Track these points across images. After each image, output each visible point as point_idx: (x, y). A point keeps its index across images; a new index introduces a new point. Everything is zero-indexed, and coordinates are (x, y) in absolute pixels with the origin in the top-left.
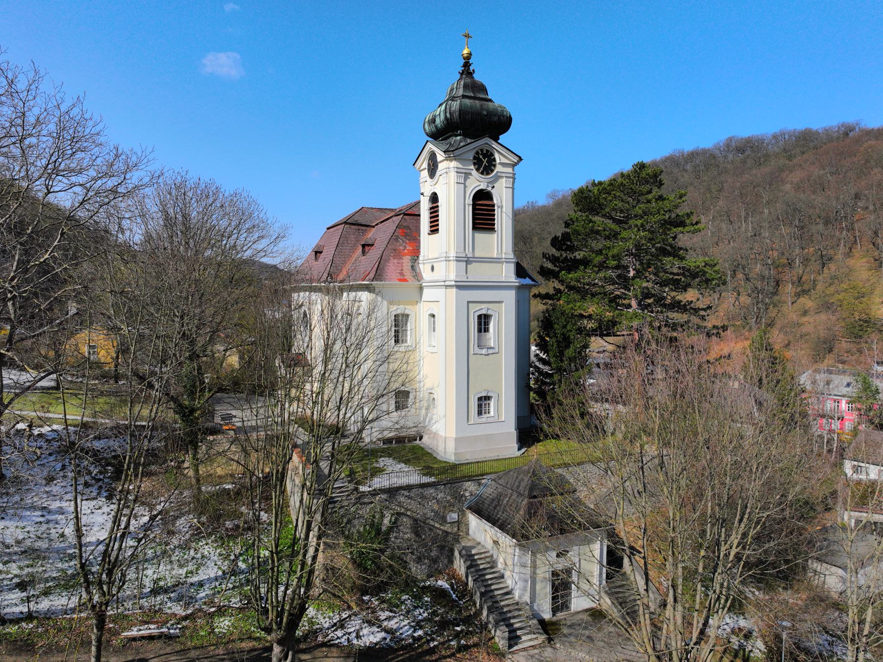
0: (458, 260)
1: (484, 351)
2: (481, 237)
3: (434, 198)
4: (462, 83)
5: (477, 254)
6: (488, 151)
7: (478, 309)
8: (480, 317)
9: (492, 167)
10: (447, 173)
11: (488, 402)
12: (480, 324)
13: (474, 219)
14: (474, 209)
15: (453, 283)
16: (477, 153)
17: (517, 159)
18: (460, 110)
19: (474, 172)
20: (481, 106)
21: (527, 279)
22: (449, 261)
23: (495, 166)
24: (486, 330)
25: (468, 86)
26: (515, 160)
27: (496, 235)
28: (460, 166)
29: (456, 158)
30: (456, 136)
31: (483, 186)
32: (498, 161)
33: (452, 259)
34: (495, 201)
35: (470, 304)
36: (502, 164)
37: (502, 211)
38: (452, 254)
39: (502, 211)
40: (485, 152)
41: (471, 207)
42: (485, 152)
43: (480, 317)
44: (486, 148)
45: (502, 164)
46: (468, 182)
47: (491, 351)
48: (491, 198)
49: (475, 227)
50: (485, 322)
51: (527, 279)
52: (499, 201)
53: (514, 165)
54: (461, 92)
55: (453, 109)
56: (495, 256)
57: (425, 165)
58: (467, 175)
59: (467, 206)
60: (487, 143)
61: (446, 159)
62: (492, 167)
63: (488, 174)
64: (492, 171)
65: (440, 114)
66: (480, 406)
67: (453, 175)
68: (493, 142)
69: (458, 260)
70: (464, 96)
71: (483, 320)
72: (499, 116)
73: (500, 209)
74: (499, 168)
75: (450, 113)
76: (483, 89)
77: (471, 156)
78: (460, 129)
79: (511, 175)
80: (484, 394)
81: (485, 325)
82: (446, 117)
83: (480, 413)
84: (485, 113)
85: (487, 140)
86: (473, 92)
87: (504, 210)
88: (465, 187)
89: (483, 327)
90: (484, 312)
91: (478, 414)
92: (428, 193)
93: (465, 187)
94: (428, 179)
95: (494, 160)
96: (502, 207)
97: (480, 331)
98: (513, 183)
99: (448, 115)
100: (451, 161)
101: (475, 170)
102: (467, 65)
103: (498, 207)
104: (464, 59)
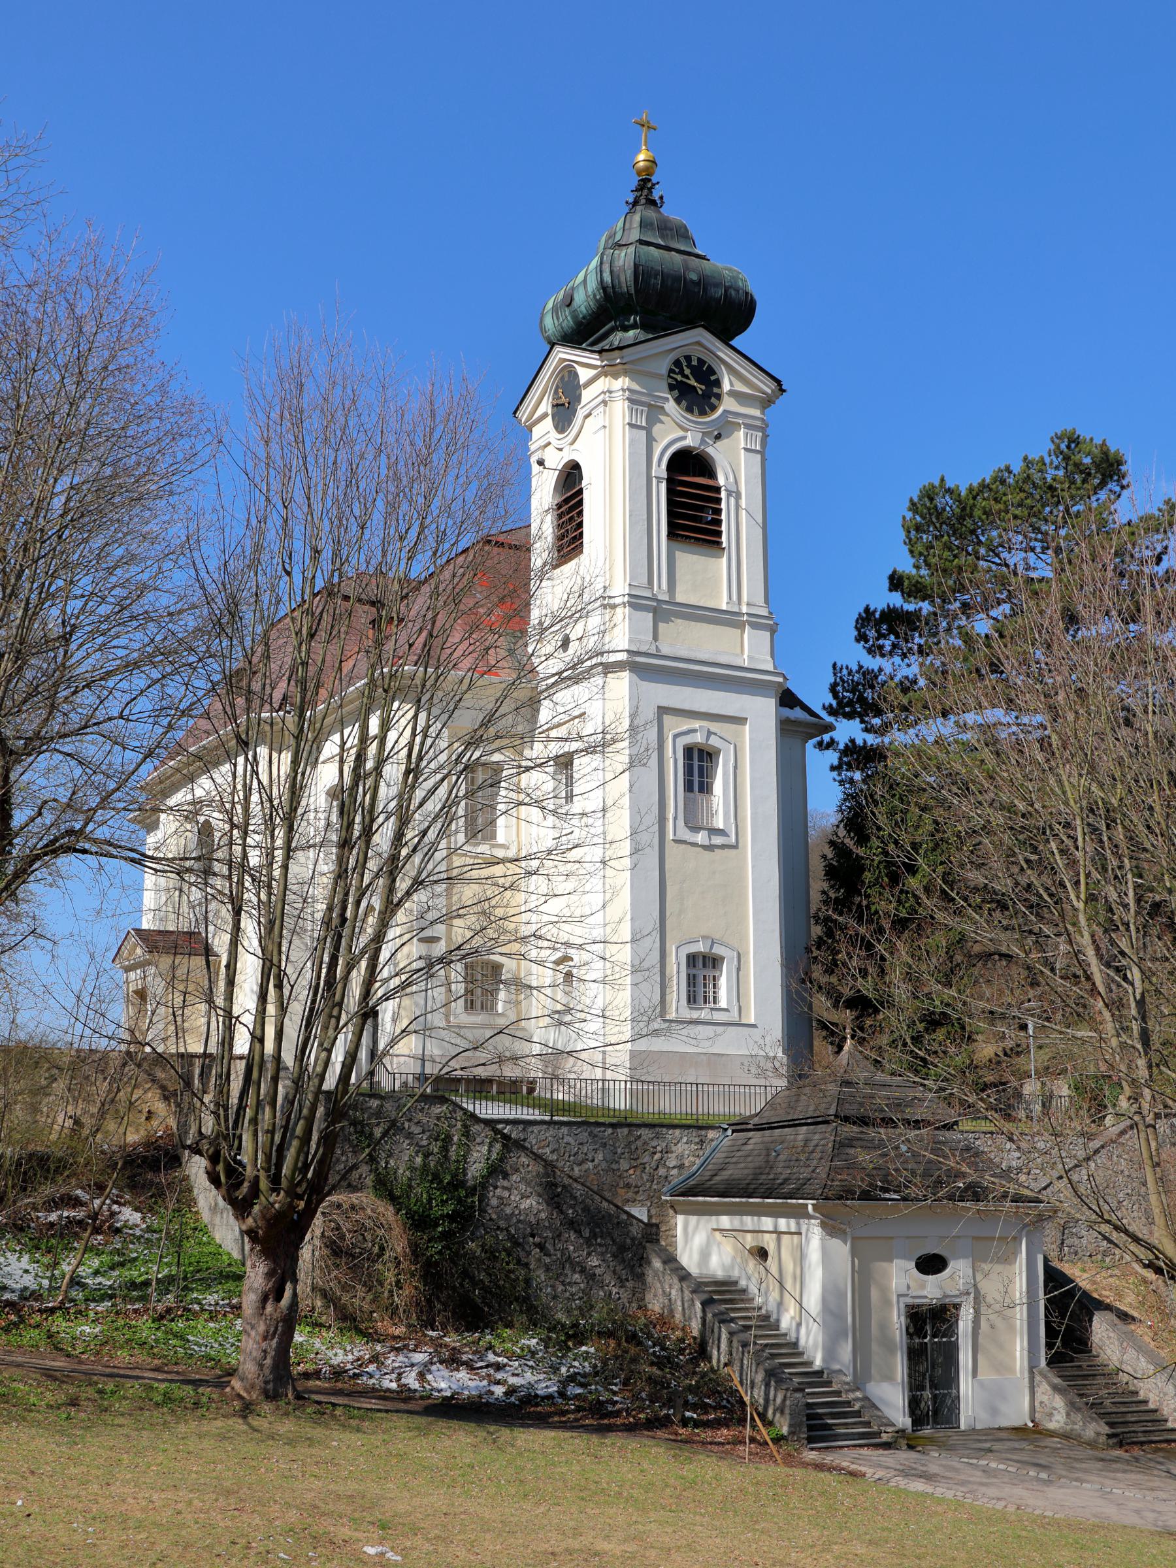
0: (635, 603)
1: (701, 838)
2: (690, 561)
3: (571, 475)
4: (637, 218)
5: (680, 598)
6: (701, 362)
7: (685, 728)
8: (689, 751)
9: (713, 400)
10: (605, 402)
11: (710, 973)
12: (689, 771)
13: (671, 514)
14: (670, 491)
15: (622, 656)
16: (677, 363)
17: (773, 385)
18: (636, 266)
19: (671, 406)
20: (685, 263)
21: (798, 709)
22: (614, 607)
23: (719, 397)
24: (705, 788)
25: (651, 224)
26: (768, 387)
27: (724, 560)
28: (636, 387)
29: (624, 370)
30: (626, 329)
31: (691, 441)
32: (726, 386)
33: (618, 601)
34: (721, 481)
35: (668, 719)
36: (733, 394)
37: (737, 506)
38: (620, 589)
39: (737, 506)
40: (695, 363)
41: (663, 486)
42: (695, 363)
43: (689, 751)
44: (697, 353)
45: (733, 394)
46: (657, 429)
47: (718, 840)
48: (712, 475)
49: (675, 532)
50: (701, 768)
51: (798, 709)
52: (731, 479)
53: (766, 402)
54: (635, 235)
55: (619, 263)
56: (724, 607)
57: (546, 407)
58: (654, 412)
59: (654, 481)
60: (698, 343)
61: (604, 372)
62: (713, 400)
63: (703, 413)
64: (714, 408)
65: (585, 281)
66: (692, 981)
67: (620, 409)
68: (719, 344)
69: (635, 603)
70: (641, 242)
71: (696, 763)
72: (727, 289)
73: (732, 500)
74: (728, 404)
75: (612, 272)
76: (682, 233)
77: (664, 366)
78: (636, 314)
79: (759, 423)
80: (700, 947)
81: (701, 775)
82: (603, 286)
83: (692, 999)
84: (694, 277)
85: (700, 335)
86: (662, 237)
87: (743, 503)
88: (650, 440)
89: (696, 779)
90: (698, 738)
91: (689, 1001)
92: (556, 460)
93: (650, 440)
94: (554, 435)
95: (718, 383)
96: (738, 496)
97: (689, 787)
98: (764, 443)
99: (607, 278)
100: (616, 376)
101: (671, 400)
102: (645, 185)
103: (729, 493)
104: (639, 174)
